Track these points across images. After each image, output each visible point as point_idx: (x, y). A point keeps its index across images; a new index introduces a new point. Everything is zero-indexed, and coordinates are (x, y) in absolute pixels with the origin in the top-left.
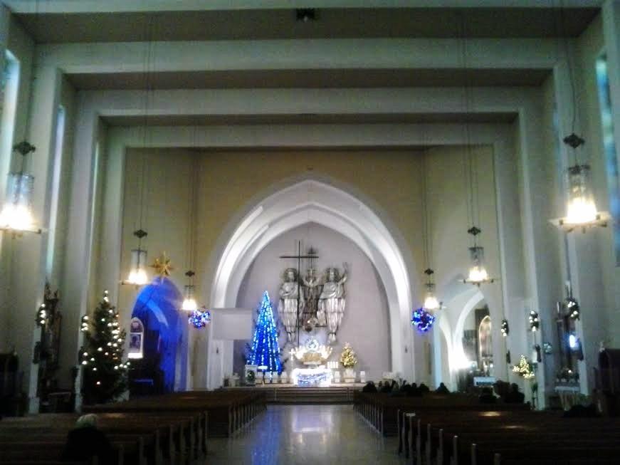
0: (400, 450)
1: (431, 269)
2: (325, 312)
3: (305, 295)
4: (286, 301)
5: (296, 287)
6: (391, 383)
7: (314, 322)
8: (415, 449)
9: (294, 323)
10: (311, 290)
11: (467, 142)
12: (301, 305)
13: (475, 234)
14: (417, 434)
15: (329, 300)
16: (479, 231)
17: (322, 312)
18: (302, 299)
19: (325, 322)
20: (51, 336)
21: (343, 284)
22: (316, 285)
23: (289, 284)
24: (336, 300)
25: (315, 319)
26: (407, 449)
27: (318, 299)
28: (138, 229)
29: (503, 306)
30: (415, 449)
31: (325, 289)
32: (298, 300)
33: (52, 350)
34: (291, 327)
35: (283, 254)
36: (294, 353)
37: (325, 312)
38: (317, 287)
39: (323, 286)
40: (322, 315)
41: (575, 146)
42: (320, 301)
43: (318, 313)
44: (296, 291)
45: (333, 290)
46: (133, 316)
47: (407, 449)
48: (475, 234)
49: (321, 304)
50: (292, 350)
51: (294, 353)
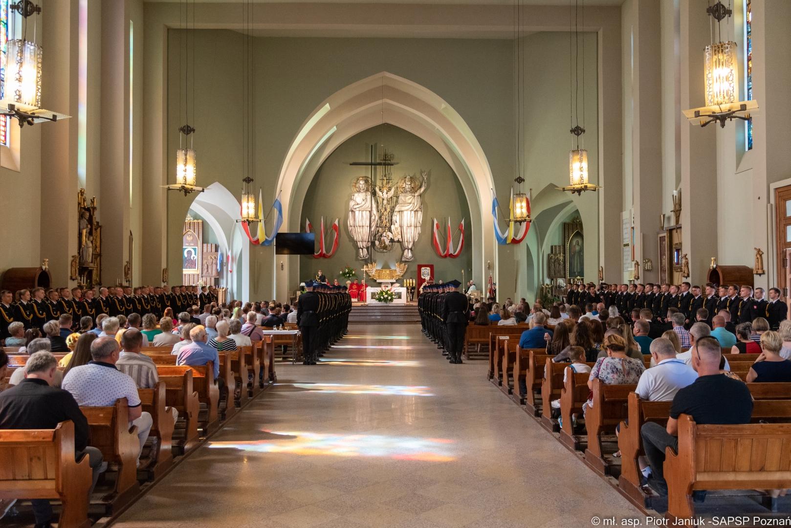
0: (491, 376)
1: (522, 177)
2: (401, 227)
3: (378, 207)
4: (357, 213)
5: (369, 197)
6: (44, 345)
7: (388, 236)
8: (500, 369)
9: (366, 237)
10: (385, 202)
11: (574, 29)
12: (373, 218)
13: (578, 135)
14: (515, 361)
15: (405, 213)
16: (523, 180)
17: (397, 225)
18: (374, 211)
19: (400, 237)
20: (91, 250)
21: (420, 195)
22: (391, 196)
23: (360, 194)
24: (413, 212)
25: (389, 233)
26: (501, 376)
27: (392, 211)
28: (184, 124)
29: (355, 316)
30: (510, 376)
31: (400, 201)
32: (370, 212)
33: (92, 265)
34: (362, 241)
35: (351, 162)
36: (367, 269)
37: (401, 227)
38: (391, 198)
39: (398, 197)
40: (396, 229)
41: (520, 178)
42: (395, 214)
43: (393, 227)
44: (368, 204)
45: (410, 201)
46: (461, 362)
47: (501, 376)
48: (578, 135)
49: (396, 217)
50: (365, 267)
51: (367, 269)
